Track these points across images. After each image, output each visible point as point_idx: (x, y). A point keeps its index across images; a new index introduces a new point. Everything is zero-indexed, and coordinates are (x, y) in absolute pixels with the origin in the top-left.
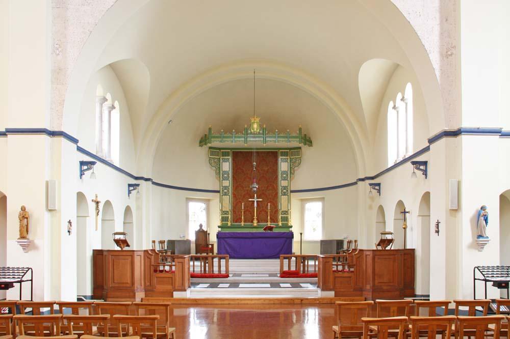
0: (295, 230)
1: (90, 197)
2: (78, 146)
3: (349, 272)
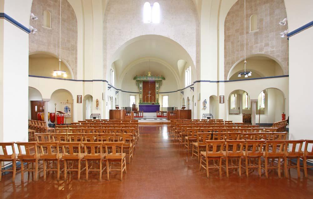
0: (160, 104)
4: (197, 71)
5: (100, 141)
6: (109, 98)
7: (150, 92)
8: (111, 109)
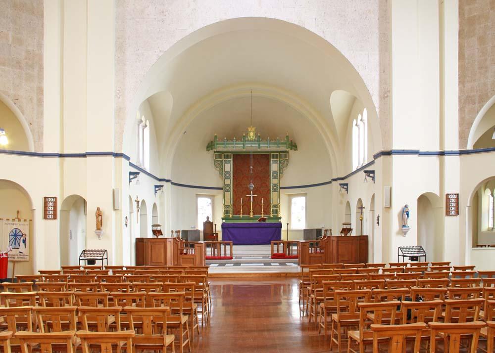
0: (283, 221)
1: (134, 199)
2: (130, 162)
3: (321, 253)
4: (383, 123)
5: (125, 327)
6: (135, 204)
7: (252, 186)
8: (139, 237)
